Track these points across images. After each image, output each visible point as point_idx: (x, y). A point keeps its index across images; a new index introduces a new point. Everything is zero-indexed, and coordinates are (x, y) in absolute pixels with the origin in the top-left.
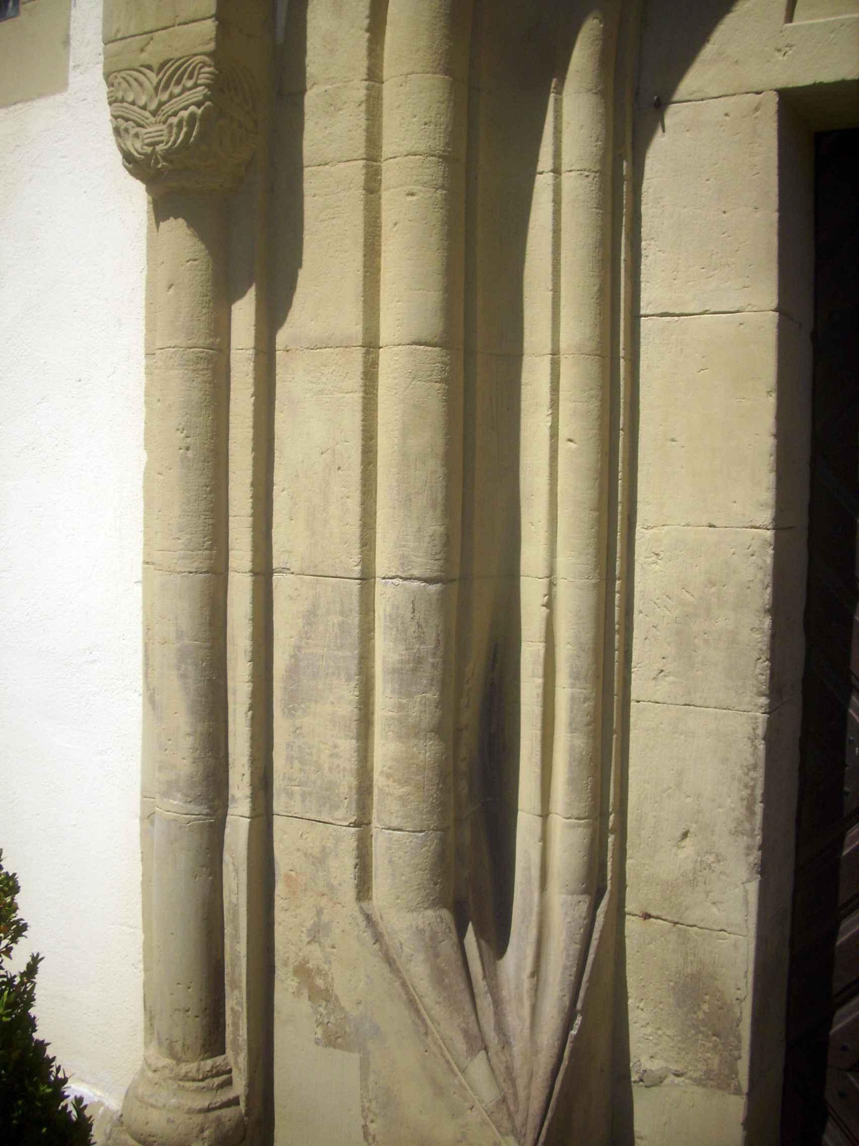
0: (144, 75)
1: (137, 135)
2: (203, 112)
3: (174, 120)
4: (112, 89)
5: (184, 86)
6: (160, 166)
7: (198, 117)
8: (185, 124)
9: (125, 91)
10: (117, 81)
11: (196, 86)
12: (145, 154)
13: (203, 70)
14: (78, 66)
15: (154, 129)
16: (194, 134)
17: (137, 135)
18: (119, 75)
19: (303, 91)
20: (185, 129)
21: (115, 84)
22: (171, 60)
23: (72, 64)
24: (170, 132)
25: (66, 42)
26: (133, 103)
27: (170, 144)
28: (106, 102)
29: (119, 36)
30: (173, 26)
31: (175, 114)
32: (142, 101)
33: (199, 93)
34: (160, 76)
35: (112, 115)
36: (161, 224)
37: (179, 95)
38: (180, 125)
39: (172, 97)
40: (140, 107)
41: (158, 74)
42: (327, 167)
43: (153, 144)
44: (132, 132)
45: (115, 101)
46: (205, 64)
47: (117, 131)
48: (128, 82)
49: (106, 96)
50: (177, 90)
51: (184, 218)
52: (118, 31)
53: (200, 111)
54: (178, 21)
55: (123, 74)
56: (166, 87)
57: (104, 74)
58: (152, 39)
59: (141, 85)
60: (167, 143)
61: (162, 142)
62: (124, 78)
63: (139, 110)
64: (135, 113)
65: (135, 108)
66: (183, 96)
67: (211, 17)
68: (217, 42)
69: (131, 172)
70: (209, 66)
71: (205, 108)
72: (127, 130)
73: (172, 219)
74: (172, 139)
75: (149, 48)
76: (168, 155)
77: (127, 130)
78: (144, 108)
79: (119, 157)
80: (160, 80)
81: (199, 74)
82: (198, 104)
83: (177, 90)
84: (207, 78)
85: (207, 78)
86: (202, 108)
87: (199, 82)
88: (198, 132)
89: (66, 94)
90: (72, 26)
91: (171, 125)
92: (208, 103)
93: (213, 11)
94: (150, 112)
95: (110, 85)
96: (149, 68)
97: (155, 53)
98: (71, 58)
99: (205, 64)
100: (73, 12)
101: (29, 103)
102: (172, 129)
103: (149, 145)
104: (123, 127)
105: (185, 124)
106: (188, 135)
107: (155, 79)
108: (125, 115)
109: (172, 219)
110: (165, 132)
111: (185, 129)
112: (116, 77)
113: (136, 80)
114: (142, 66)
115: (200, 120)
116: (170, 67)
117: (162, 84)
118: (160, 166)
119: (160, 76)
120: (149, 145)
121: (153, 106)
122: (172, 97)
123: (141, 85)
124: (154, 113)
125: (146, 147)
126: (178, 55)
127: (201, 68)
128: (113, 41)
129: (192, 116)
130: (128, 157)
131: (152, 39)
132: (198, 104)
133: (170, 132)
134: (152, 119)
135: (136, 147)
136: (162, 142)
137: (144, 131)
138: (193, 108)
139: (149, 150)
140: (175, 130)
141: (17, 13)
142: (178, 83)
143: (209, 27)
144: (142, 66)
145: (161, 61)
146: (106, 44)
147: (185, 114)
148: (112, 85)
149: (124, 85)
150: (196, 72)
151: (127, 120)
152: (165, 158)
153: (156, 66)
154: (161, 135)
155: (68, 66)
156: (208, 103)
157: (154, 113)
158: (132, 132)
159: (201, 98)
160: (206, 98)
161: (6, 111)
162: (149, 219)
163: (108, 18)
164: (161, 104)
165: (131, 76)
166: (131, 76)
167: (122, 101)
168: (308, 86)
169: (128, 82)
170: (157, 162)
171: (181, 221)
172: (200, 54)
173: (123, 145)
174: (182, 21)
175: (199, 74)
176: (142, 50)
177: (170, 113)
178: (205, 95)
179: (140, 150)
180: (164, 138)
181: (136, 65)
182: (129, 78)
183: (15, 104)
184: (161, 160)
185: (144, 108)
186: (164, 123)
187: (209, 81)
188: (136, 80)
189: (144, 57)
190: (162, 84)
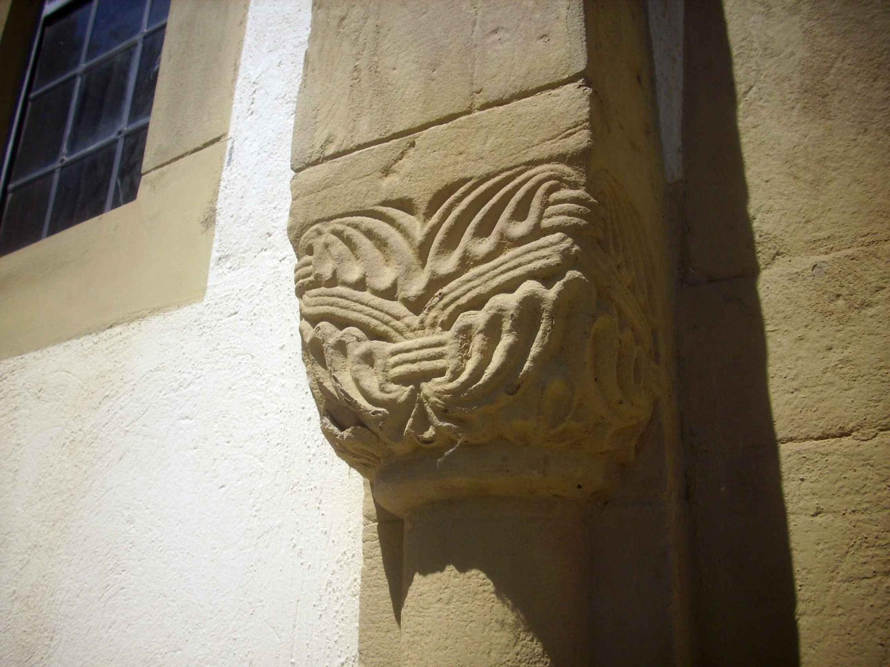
0: (391, 221)
1: (368, 358)
2: (560, 293)
3: (479, 318)
4: (307, 258)
5: (502, 235)
6: (430, 433)
7: (547, 306)
8: (507, 325)
9: (340, 260)
10: (322, 240)
11: (537, 232)
12: (390, 404)
13: (555, 196)
14: (227, 257)
15: (416, 341)
16: (534, 350)
17: (368, 358)
18: (326, 228)
19: (752, 272)
20: (506, 340)
21: (318, 248)
22: (464, 181)
23: (215, 255)
24: (464, 349)
25: (209, 221)
26: (360, 285)
27: (464, 377)
28: (293, 287)
29: (331, 150)
30: (468, 112)
31: (477, 303)
32: (385, 278)
33: (550, 249)
34: (435, 219)
35: (304, 316)
36: (421, 586)
37: (489, 257)
38: (493, 329)
39: (466, 262)
40: (377, 293)
41: (428, 215)
42: (845, 440)
43: (414, 379)
44: (357, 349)
45: (317, 283)
46: (560, 182)
47: (314, 351)
48: (348, 241)
49: (292, 276)
50: (485, 246)
51: (482, 569)
52: (328, 141)
53: (551, 294)
54: (480, 100)
55: (336, 224)
56: (451, 242)
57: (290, 229)
58: (413, 145)
59: (381, 243)
60: (456, 374)
61: (441, 372)
62: (338, 234)
63: (377, 301)
64: (366, 306)
65: (367, 296)
66: (502, 258)
67: (571, 80)
68: (592, 128)
69: (342, 449)
70: (574, 186)
71: (565, 284)
72: (341, 347)
73: (450, 570)
74: (470, 365)
75: (406, 164)
76: (453, 405)
77: (341, 347)
78: (390, 293)
79: (312, 410)
80: (435, 229)
81: (545, 205)
82: (546, 277)
83: (485, 246)
84: (570, 214)
85: (570, 214)
86: (558, 286)
87: (545, 223)
88: (545, 348)
89: (199, 307)
90: (221, 195)
91: (466, 332)
92: (571, 274)
93: (580, 64)
94: (406, 302)
95: (303, 249)
96: (406, 205)
97: (416, 174)
98: (216, 245)
99: (560, 182)
100: (225, 174)
101: (135, 324)
102: (470, 339)
103: (401, 380)
104: (331, 341)
105: (507, 325)
106: (516, 353)
107: (418, 228)
108: (340, 312)
109: (450, 570)
110: (451, 349)
111: (506, 340)
112: (319, 233)
113: (369, 234)
114: (385, 203)
115: (551, 317)
116: (459, 200)
117: (439, 237)
118: (430, 433)
119: (435, 219)
120: (401, 380)
121: (415, 287)
122: (466, 262)
123: (381, 243)
124: (416, 305)
125: (393, 387)
126: (484, 168)
127: (550, 191)
128: (316, 163)
129: (531, 305)
130: (337, 412)
131: (413, 145)
132: (546, 277)
133: (464, 349)
134: (414, 320)
135: (365, 385)
136: (441, 372)
137: (390, 347)
138: (530, 286)
139: (401, 393)
140: (477, 342)
141: (130, 194)
142: (483, 231)
143: (573, 101)
144: (385, 203)
145: (436, 185)
146: (297, 171)
147: (510, 301)
148: (310, 250)
149: (340, 247)
150: (536, 203)
151: (341, 323)
152: (443, 414)
153: (422, 201)
154: (440, 356)
155: (208, 255)
156: (571, 274)
157: (416, 305)
158: (357, 349)
159: (555, 259)
160: (569, 260)
161: (96, 339)
162: (367, 557)
163: (305, 122)
164: (436, 283)
165: (356, 227)
166: (356, 227)
167: (334, 281)
168: (762, 258)
169: (348, 241)
170: (423, 421)
171: (477, 578)
172: (549, 160)
173: (328, 384)
174: (494, 96)
175: (545, 205)
176: (387, 171)
177: (463, 300)
178: (565, 253)
179: (378, 394)
180: (448, 363)
181: (369, 203)
182: (350, 231)
183: (111, 327)
184: (434, 418)
185: (390, 293)
186: (446, 326)
187: (576, 220)
188: (369, 234)
189: (392, 186)
190: (439, 237)
